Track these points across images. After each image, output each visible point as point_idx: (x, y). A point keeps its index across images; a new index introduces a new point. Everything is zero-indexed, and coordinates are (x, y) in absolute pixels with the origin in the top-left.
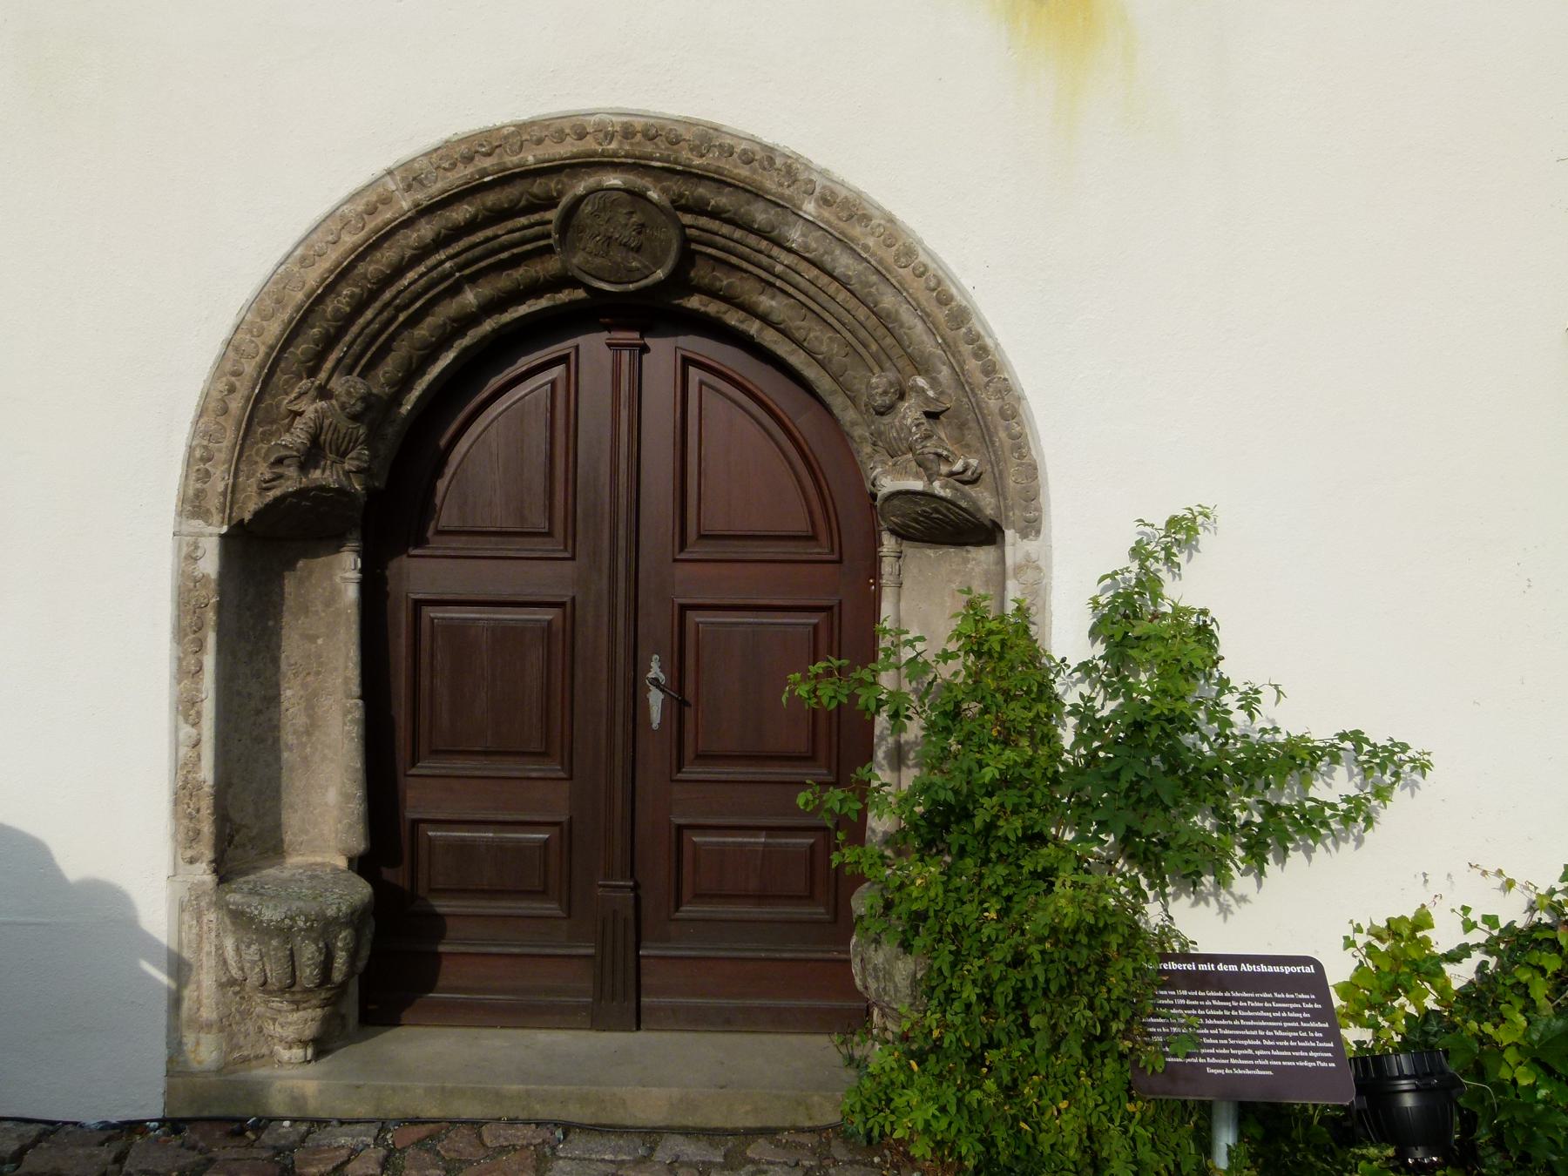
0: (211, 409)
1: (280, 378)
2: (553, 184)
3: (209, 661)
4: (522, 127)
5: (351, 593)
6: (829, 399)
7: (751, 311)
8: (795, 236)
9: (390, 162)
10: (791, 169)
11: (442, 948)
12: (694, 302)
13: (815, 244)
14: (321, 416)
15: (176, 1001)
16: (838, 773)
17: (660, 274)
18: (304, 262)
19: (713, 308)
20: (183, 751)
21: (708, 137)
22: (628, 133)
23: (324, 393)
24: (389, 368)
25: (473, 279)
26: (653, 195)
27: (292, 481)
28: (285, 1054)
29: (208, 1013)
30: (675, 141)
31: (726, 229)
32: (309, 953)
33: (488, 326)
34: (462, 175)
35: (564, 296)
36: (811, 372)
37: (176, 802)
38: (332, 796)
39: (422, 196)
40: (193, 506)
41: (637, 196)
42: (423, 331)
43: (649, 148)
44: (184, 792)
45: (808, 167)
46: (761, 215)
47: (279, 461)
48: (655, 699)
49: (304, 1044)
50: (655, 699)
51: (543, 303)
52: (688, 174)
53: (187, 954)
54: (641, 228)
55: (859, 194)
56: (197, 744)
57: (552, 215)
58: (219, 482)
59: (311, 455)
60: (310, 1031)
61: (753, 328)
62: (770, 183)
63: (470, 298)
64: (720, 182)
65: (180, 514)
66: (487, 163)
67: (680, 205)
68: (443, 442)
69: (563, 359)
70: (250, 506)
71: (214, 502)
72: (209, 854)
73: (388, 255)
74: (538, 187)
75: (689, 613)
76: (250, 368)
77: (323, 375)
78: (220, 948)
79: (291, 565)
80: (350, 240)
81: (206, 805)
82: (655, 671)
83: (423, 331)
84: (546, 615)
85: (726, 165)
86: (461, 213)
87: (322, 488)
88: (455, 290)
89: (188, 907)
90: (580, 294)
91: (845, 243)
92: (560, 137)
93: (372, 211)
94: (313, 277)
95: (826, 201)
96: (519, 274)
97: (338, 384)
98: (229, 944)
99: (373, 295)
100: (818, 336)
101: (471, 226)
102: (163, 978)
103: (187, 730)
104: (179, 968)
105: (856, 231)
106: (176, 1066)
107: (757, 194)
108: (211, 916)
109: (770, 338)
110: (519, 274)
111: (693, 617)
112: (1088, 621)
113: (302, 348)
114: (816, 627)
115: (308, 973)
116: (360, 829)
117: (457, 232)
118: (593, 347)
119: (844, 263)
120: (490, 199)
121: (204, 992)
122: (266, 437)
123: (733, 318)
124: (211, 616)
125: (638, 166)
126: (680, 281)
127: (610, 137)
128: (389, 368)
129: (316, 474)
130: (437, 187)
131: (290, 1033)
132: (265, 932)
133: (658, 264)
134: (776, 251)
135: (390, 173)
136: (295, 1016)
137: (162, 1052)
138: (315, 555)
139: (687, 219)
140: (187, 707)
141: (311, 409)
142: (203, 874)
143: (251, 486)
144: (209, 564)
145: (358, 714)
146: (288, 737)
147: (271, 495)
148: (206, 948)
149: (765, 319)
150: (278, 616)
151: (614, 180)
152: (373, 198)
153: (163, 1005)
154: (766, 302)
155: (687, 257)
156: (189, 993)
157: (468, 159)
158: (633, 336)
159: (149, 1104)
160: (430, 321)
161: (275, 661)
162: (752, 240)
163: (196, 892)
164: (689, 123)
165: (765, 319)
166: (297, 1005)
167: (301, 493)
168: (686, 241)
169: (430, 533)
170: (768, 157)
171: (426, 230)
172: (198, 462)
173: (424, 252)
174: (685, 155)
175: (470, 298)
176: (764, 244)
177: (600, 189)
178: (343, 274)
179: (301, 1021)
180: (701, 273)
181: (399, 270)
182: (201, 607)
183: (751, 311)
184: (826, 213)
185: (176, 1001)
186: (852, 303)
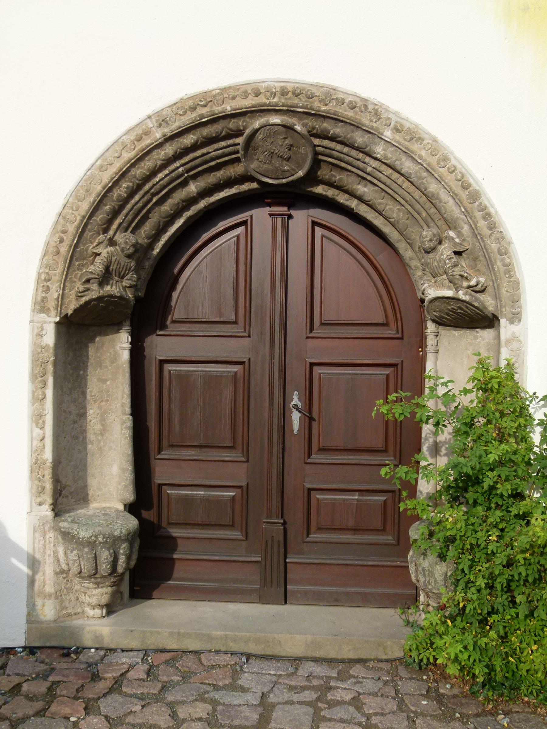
1: (88, 234)
3: (49, 392)
4: (223, 90)
5: (125, 356)
7: (352, 194)
8: (379, 150)
11: (175, 556)
12: (320, 189)
14: (111, 255)
15: (32, 582)
17: (301, 174)
18: (101, 168)
19: (330, 193)
20: (35, 443)
22: (284, 92)
24: (147, 228)
25: (194, 177)
26: (298, 128)
27: (95, 292)
29: (49, 589)
32: (105, 555)
33: (202, 204)
35: (246, 187)
36: (387, 229)
38: (115, 469)
39: (167, 131)
41: (289, 128)
43: (296, 101)
46: (359, 139)
47: (88, 281)
48: (296, 416)
49: (101, 607)
50: (296, 416)
51: (233, 191)
52: (318, 116)
53: (38, 556)
57: (240, 140)
58: (55, 293)
61: (353, 204)
62: (365, 120)
63: (193, 188)
65: (33, 311)
66: (204, 111)
68: (176, 271)
70: (71, 307)
71: (52, 304)
72: (49, 500)
73: (148, 164)
74: (232, 124)
77: (111, 232)
78: (55, 552)
79: (92, 340)
80: (127, 156)
81: (48, 473)
82: (296, 401)
87: (111, 296)
88: (184, 184)
90: (255, 185)
91: (408, 154)
92: (246, 95)
95: (397, 130)
96: (221, 174)
97: (120, 238)
98: (61, 550)
99: (139, 187)
101: (195, 147)
103: (37, 431)
107: (357, 127)
108: (51, 535)
109: (363, 210)
110: (221, 174)
113: (100, 217)
114: (388, 376)
115: (104, 567)
117: (187, 151)
119: (407, 166)
120: (206, 131)
122: (80, 267)
123: (342, 198)
124: (50, 368)
125: (290, 111)
127: (274, 95)
128: (147, 228)
129: (108, 288)
130: (176, 125)
131: (94, 601)
132: (80, 543)
136: (97, 591)
137: (24, 610)
138: (101, 334)
139: (317, 141)
141: (105, 251)
142: (46, 511)
143: (72, 295)
144: (50, 339)
145: (129, 424)
146: (91, 436)
148: (48, 552)
149: (360, 199)
150: (85, 368)
151: (275, 119)
153: (24, 584)
154: (362, 189)
155: (316, 163)
156: (37, 577)
157: (193, 109)
158: (283, 210)
161: (84, 394)
162: (354, 153)
163: (43, 522)
164: (318, 86)
165: (360, 199)
167: (100, 299)
168: (316, 154)
169: (168, 322)
171: (169, 150)
173: (168, 162)
174: (316, 104)
175: (193, 188)
176: (361, 155)
180: (324, 173)
181: (154, 173)
183: (352, 194)
184: (398, 137)
185: (32, 582)
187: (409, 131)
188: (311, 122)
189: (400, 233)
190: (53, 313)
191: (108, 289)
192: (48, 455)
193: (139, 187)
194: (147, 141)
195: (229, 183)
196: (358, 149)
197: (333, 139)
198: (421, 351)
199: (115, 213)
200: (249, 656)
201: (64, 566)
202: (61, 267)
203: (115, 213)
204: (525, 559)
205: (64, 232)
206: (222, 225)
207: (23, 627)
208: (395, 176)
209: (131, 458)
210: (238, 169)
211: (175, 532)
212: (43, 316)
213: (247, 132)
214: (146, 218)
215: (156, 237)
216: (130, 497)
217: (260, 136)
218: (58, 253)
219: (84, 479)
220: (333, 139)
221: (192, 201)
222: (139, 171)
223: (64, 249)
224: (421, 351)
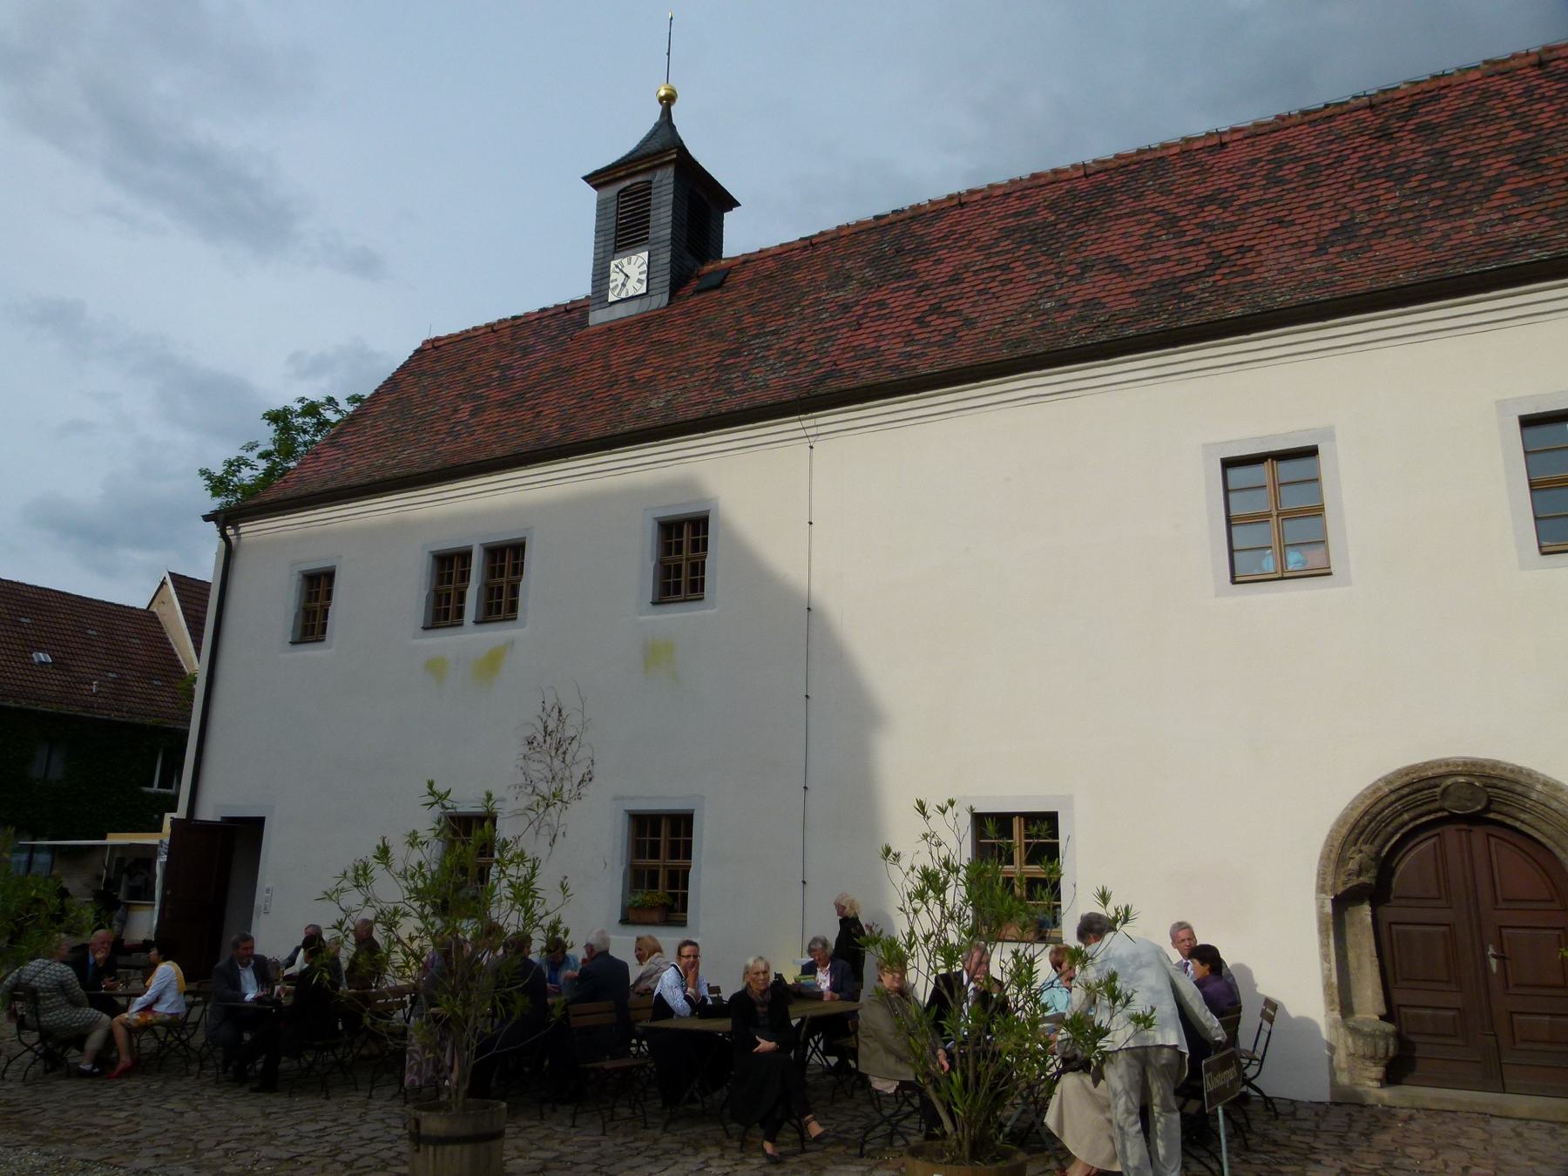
0: (1325, 858)
1: (1346, 847)
2: (1437, 781)
3: (1332, 942)
4: (1426, 763)
5: (1369, 919)
6: (1553, 850)
7: (1517, 819)
8: (1534, 796)
9: (1379, 777)
10: (1530, 774)
11: (1416, 1055)
12: (1492, 816)
13: (1542, 798)
14: (1362, 859)
15: (1331, 1060)
16: (1512, 1023)
17: (1479, 808)
18: (1352, 809)
19: (1499, 817)
20: (1326, 972)
21: (1495, 765)
22: (1465, 764)
23: (1361, 851)
24: (1378, 842)
25: (1407, 811)
26: (1477, 784)
27: (1355, 881)
28: (1371, 1084)
29: (1343, 1065)
30: (1484, 766)
31: (1505, 793)
32: (1381, 1043)
33: (1411, 825)
34: (1406, 779)
35: (1440, 814)
36: (1544, 840)
37: (1325, 990)
38: (1369, 993)
39: (1392, 787)
40: (1321, 889)
41: (1472, 784)
42: (1389, 829)
43: (1474, 769)
44: (1327, 986)
45: (1536, 773)
46: (1519, 789)
47: (1349, 875)
48: (1494, 963)
49: (1377, 1080)
50: (1494, 963)
51: (1432, 817)
52: (1489, 777)
53: (1334, 1043)
54: (1471, 794)
55: (1558, 782)
56: (1330, 970)
57: (1438, 790)
58: (1330, 881)
59: (1359, 873)
60: (1380, 1076)
61: (1518, 824)
62: (1522, 779)
63: (1406, 817)
64: (1502, 779)
65: (1317, 891)
66: (1414, 775)
67: (1486, 786)
68: (1394, 865)
69: (1439, 834)
70: (1340, 890)
71: (1328, 888)
72: (1338, 1008)
73: (1381, 805)
74: (1432, 782)
75: (1503, 930)
76: (1336, 844)
77: (1358, 844)
78: (1345, 1042)
79: (1347, 909)
80: (1368, 802)
81: (1336, 991)
82: (1491, 951)
83: (1389, 829)
84: (1442, 929)
85: (1504, 773)
86: (1406, 790)
87: (1364, 884)
88: (1401, 814)
89: (1333, 1026)
90: (1446, 813)
91: (1556, 799)
92: (1440, 766)
93: (1374, 792)
94: (1356, 814)
95: (1545, 784)
96: (1424, 808)
97: (1365, 848)
98: (1350, 1040)
99: (1375, 818)
100: (1544, 827)
101: (1408, 795)
102: (1327, 1052)
103: (1326, 965)
104: (1332, 1049)
105: (1559, 794)
106: (1334, 1084)
107: (1517, 782)
108: (1342, 1030)
109: (1525, 828)
110: (1424, 808)
111: (1504, 931)
112: (210, 492)
113: (1353, 837)
114: (1559, 935)
115: (1381, 1052)
116: (1383, 1005)
117: (1403, 797)
118: (1450, 831)
119: (1555, 804)
120: (1415, 786)
121: (1341, 1057)
122: (1343, 866)
123: (1509, 821)
124: (1331, 926)
125: (1470, 775)
126: (1487, 809)
127: (1458, 766)
128: (1378, 842)
129: (1361, 879)
130: (1397, 784)
131: (1373, 1075)
132: (1364, 1035)
133: (1479, 804)
134: (1526, 800)
135: (1380, 780)
136: (1375, 1069)
137: (1327, 1077)
138: (1353, 905)
139: (1489, 790)
140: (1325, 957)
141: (1358, 857)
142: (1337, 1015)
143: (1339, 882)
144: (1329, 909)
145: (1377, 963)
146: (1352, 970)
147: (1349, 886)
148: (1340, 1041)
149: (1523, 822)
150: (1345, 928)
151: (1462, 780)
152: (1375, 788)
153: (1326, 1061)
154: (1523, 816)
155: (1490, 802)
156: (1335, 1057)
157: (1407, 775)
158: (1465, 827)
159: (1326, 1098)
160: (1392, 825)
161: (1345, 944)
162: (1516, 796)
163: (1335, 1021)
164: (1488, 760)
165: (1523, 822)
166: (1376, 1064)
167: (1358, 885)
168: (1489, 796)
169: (1392, 897)
170: (1520, 770)
171: (1393, 797)
172: (1322, 875)
173: (1392, 803)
174: (1488, 771)
175: (1406, 817)
176: (1520, 798)
177: (1457, 783)
178: (1366, 813)
179: (1377, 1071)
180: (1494, 806)
181: (1383, 810)
182: (1327, 923)
183: (1517, 819)
184: (1546, 788)
185: (1331, 1060)
186: (1560, 818)
187: (1553, 785)
188: (1484, 780)
189: (1555, 842)
190: (1329, 893)
191: (1362, 879)
192: (1334, 979)
193: (1375, 818)
194: (1380, 794)
195: (1429, 813)
196: (1518, 794)
197: (1500, 788)
198: (634, 1045)
199: (1361, 834)
200: (1492, 1116)
201: (1352, 1051)
202: (1332, 867)
203: (1361, 834)
204: (1513, 193)
205: (1332, 846)
206: (1422, 837)
207: (1328, 1090)
208: (1547, 809)
209: (1380, 986)
210: (1436, 805)
211: (1413, 1038)
212: (1323, 895)
213: (1443, 786)
214: (1378, 835)
215: (1382, 847)
216: (1383, 1011)
217: (1451, 788)
218: (1329, 858)
219: (1351, 998)
220: (1500, 788)
221: (1406, 824)
222: (1375, 810)
223: (1333, 856)
224: (634, 1045)
